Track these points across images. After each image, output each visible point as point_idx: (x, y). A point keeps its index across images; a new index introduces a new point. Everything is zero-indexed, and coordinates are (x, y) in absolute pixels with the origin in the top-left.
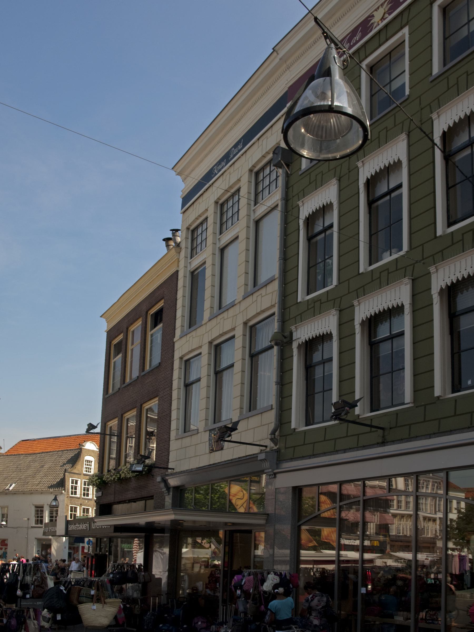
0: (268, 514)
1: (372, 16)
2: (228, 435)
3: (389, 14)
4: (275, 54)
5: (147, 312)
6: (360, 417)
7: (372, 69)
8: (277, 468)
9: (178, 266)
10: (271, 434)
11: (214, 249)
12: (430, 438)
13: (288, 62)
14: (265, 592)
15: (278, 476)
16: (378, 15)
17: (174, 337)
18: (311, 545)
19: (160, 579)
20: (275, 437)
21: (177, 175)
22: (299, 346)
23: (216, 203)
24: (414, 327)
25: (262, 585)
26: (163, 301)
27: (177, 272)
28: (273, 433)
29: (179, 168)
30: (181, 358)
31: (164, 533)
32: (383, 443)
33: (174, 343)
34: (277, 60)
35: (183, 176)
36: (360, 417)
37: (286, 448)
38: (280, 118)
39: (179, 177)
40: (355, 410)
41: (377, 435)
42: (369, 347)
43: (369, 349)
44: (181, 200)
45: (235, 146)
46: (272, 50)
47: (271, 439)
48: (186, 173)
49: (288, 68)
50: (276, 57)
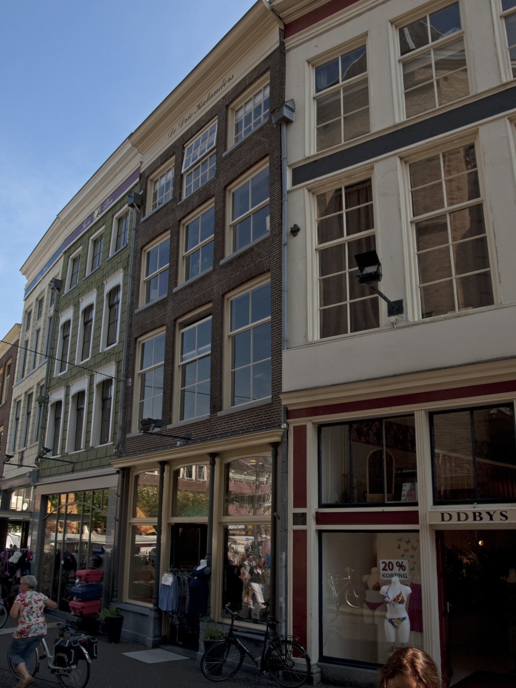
0: (31, 512)
1: (94, 212)
2: (7, 460)
3: (100, 215)
4: (58, 219)
5: (6, 363)
6: (69, 454)
7: (95, 242)
8: (37, 482)
9: (19, 336)
10: (35, 460)
11: (33, 331)
12: (103, 468)
13: (66, 224)
14: (12, 563)
15: (37, 487)
16: (96, 212)
17: (13, 385)
19: (467, 562)
20: (38, 462)
21: (23, 274)
22: (52, 406)
24: (89, 404)
25: (9, 558)
26: (11, 359)
27: (18, 340)
28: (37, 459)
29: (24, 269)
30: (15, 400)
31: (388, 493)
32: (73, 471)
33: (13, 389)
34: (59, 223)
35: (27, 275)
36: (69, 454)
37: (42, 470)
38: (60, 258)
39: (24, 276)
41: (70, 467)
42: (77, 411)
43: (77, 413)
44: (24, 291)
45: (45, 267)
46: (56, 217)
47: (35, 463)
48: (29, 273)
49: (66, 228)
50: (58, 221)
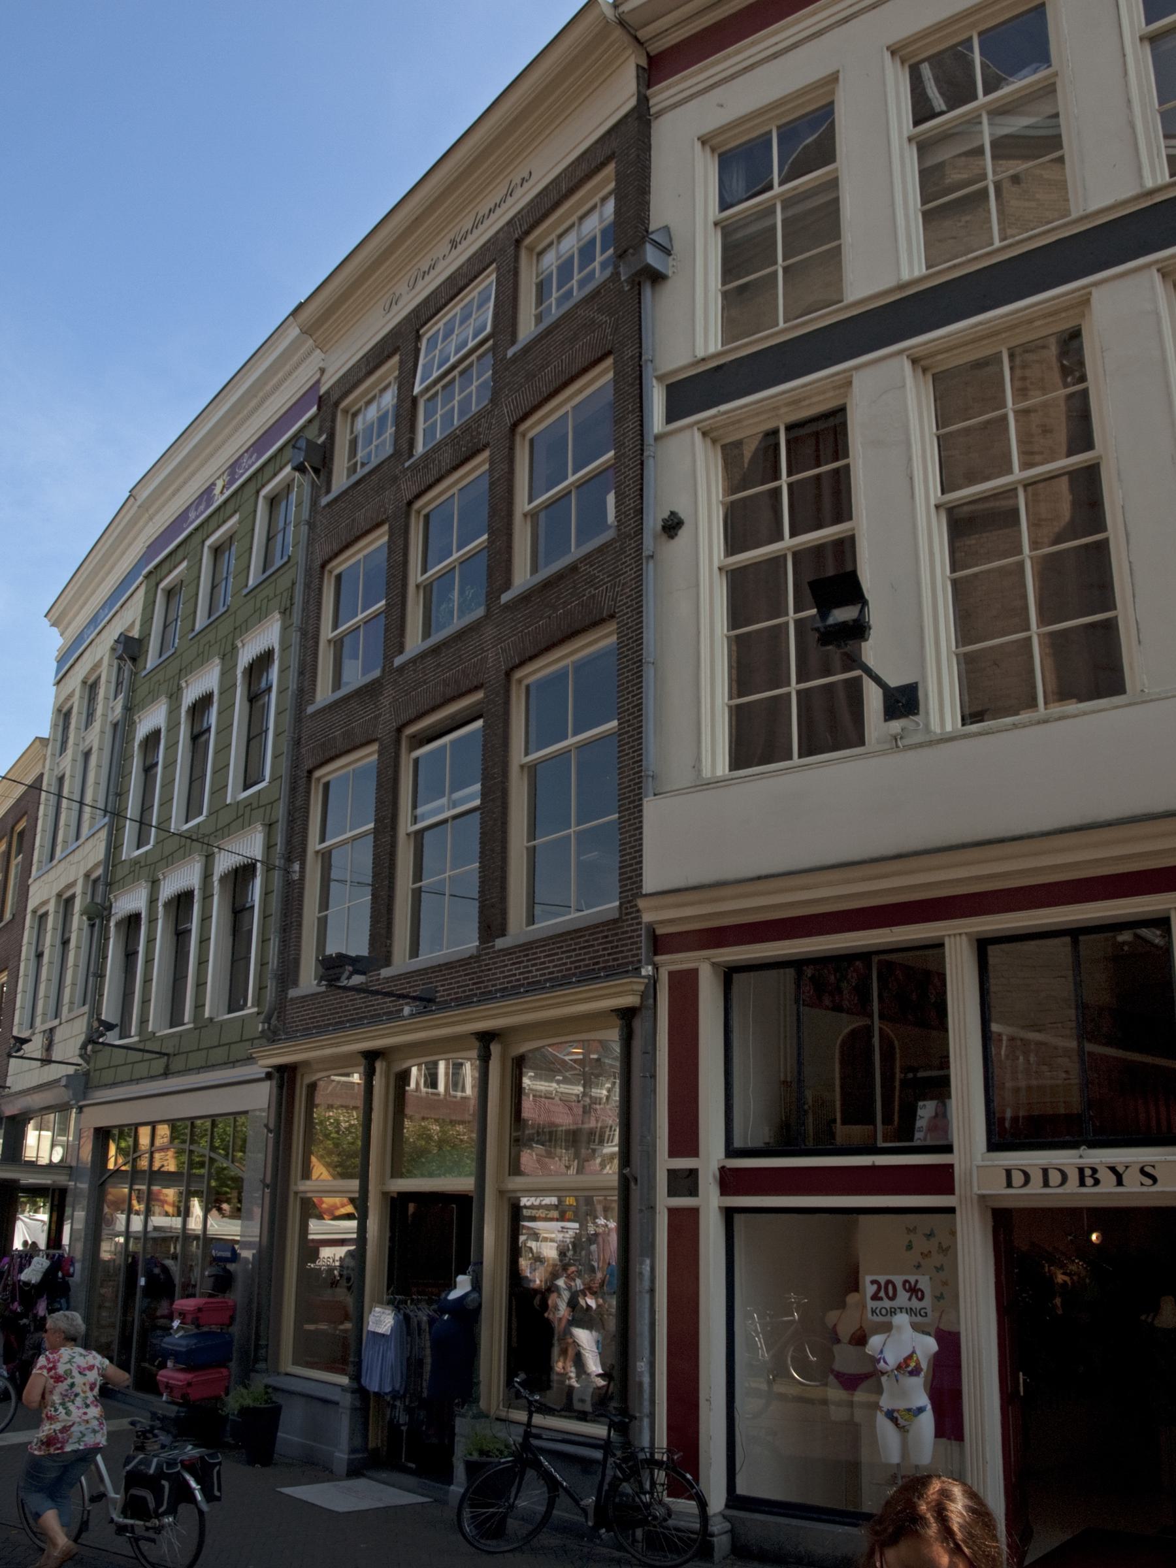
0: (71, 1167)
1: (214, 484)
2: (16, 1048)
3: (228, 489)
4: (132, 499)
5: (13, 828)
6: (157, 1035)
7: (217, 551)
8: (85, 1099)
9: (44, 767)
10: (81, 1049)
11: (75, 753)
12: (234, 1067)
13: (151, 511)
14: (27, 1284)
15: (85, 1110)
16: (220, 484)
17: (30, 877)
18: (343, 1211)
20: (86, 1053)
21: (52, 625)
22: (117, 924)
23: (84, 682)
24: (203, 920)
25: (21, 1271)
26: (25, 818)
27: (42, 775)
28: (84, 1047)
29: (55, 613)
30: (34, 912)
32: (166, 1074)
33: (29, 886)
34: (135, 508)
35: (61, 627)
36: (157, 1035)
37: (95, 1070)
38: (138, 588)
39: (55, 630)
40: (662, 935)
41: (159, 1065)
42: (175, 938)
43: (175, 942)
44: (55, 664)
45: (102, 608)
46: (128, 494)
47: (81, 1056)
48: (65, 622)
49: (151, 519)
50: (133, 504)
